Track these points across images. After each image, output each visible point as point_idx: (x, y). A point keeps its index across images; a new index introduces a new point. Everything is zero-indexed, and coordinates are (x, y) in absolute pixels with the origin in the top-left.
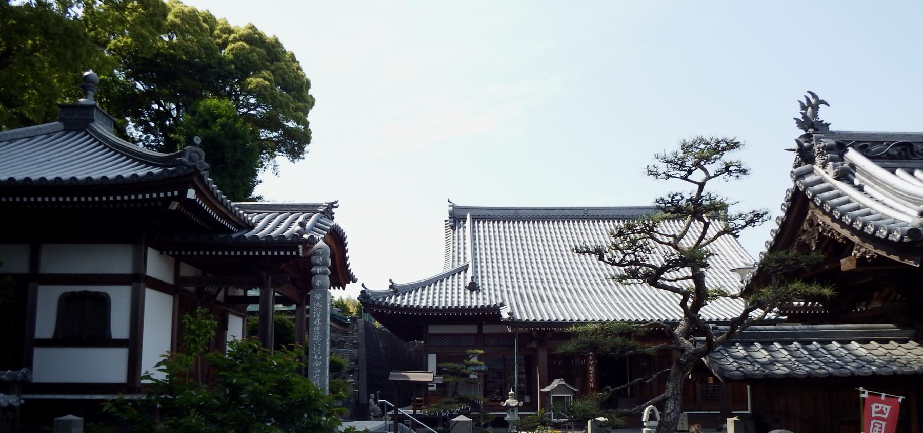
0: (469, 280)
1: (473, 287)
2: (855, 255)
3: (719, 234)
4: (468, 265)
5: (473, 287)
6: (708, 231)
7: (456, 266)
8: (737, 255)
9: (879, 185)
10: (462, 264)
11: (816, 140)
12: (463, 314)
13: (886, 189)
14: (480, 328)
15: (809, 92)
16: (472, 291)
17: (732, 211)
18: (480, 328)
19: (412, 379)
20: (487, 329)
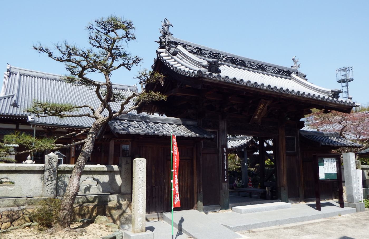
0: (13, 102)
1: (15, 105)
2: (178, 86)
3: (121, 65)
4: (14, 95)
5: (15, 105)
6: (128, 195)
7: (8, 95)
8: (129, 81)
9: (189, 59)
10: (11, 94)
11: (166, 43)
12: (7, 118)
13: (191, 60)
14: (17, 126)
15: (166, 19)
16: (14, 107)
17: (129, 57)
18: (17, 126)
19: (104, 166)
20: (21, 127)
